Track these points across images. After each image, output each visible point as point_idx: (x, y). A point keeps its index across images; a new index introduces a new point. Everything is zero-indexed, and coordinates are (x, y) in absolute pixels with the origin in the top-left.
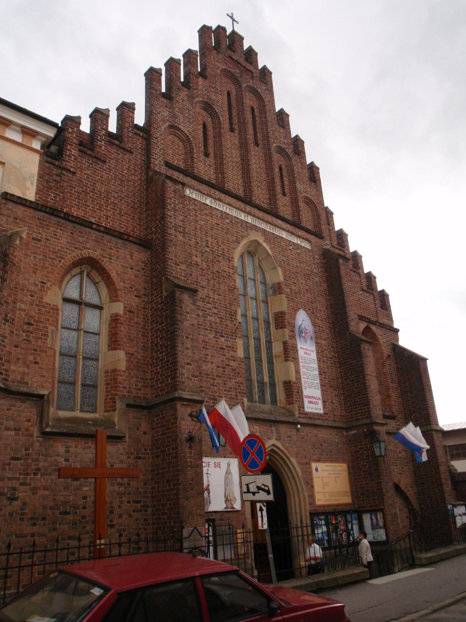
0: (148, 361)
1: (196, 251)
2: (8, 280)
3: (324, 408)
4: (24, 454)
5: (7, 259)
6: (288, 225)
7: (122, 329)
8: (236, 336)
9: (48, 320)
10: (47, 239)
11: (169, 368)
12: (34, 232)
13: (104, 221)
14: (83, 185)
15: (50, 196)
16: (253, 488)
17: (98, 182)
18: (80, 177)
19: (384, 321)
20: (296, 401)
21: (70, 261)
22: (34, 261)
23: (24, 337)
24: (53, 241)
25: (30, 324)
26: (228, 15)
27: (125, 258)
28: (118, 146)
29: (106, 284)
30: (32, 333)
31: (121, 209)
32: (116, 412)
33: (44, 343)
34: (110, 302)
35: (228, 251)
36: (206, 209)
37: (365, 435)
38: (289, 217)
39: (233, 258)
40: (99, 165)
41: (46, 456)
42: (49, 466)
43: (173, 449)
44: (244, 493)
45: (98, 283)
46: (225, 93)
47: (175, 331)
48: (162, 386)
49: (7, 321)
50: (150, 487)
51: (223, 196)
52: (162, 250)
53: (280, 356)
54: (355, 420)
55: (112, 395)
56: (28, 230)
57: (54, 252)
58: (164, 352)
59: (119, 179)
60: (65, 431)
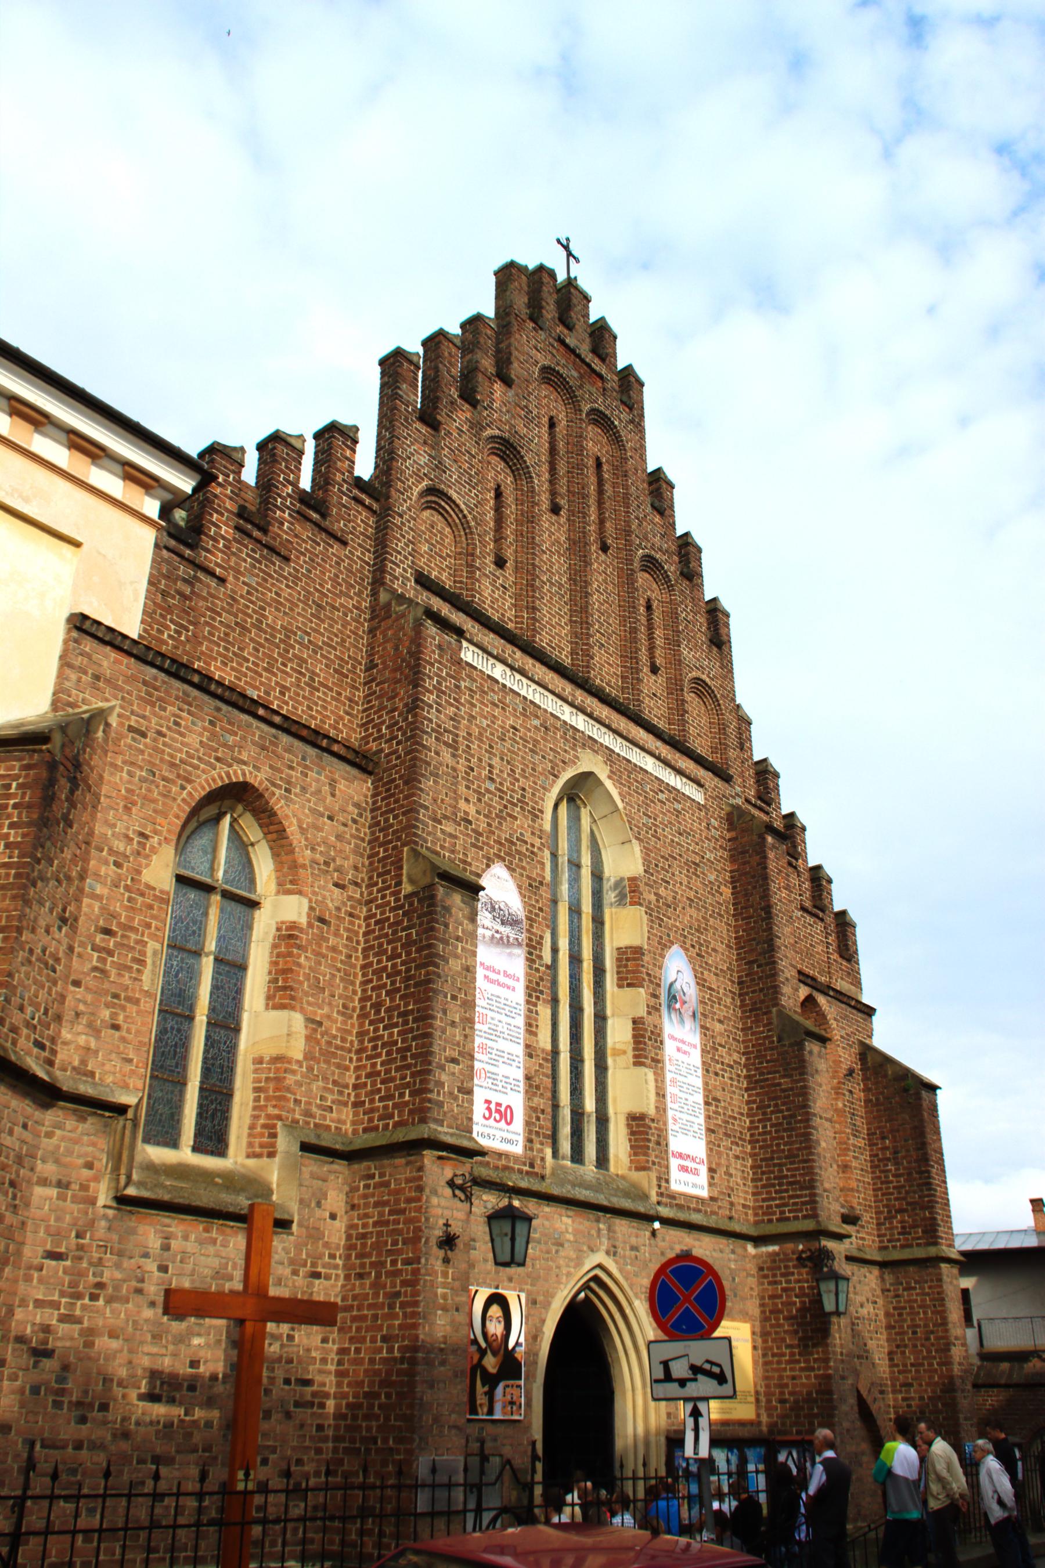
0: (352, 1042)
1: (468, 787)
2: (75, 826)
3: (710, 1185)
4: (74, 1247)
5: (78, 775)
6: (659, 744)
7: (302, 960)
8: (538, 998)
9: (148, 926)
10: (160, 733)
11: (408, 1067)
12: (133, 712)
13: (276, 698)
14: (238, 610)
15: (168, 628)
16: (679, 1369)
17: (270, 605)
18: (232, 590)
19: (842, 985)
20: (654, 1163)
21: (203, 788)
22: (129, 782)
23: (95, 963)
24: (172, 739)
25: (107, 932)
26: (559, 241)
27: (319, 791)
28: (316, 524)
29: (271, 848)
30: (110, 953)
31: (314, 673)
32: (277, 1159)
33: (136, 979)
34: (278, 893)
35: (533, 794)
36: (493, 691)
37: (799, 1258)
38: (661, 724)
39: (542, 812)
40: (274, 564)
41: (120, 1254)
42: (124, 1281)
43: (407, 1262)
44: (657, 1381)
45: (252, 845)
46: (545, 420)
47: (429, 981)
48: (386, 1107)
49: (64, 921)
50: (335, 1347)
51: (529, 663)
52: (406, 783)
53: (624, 1052)
54: (778, 1220)
55: (269, 1117)
56: (122, 707)
57: (173, 765)
58: (396, 1025)
59: (314, 602)
60: (167, 1197)
